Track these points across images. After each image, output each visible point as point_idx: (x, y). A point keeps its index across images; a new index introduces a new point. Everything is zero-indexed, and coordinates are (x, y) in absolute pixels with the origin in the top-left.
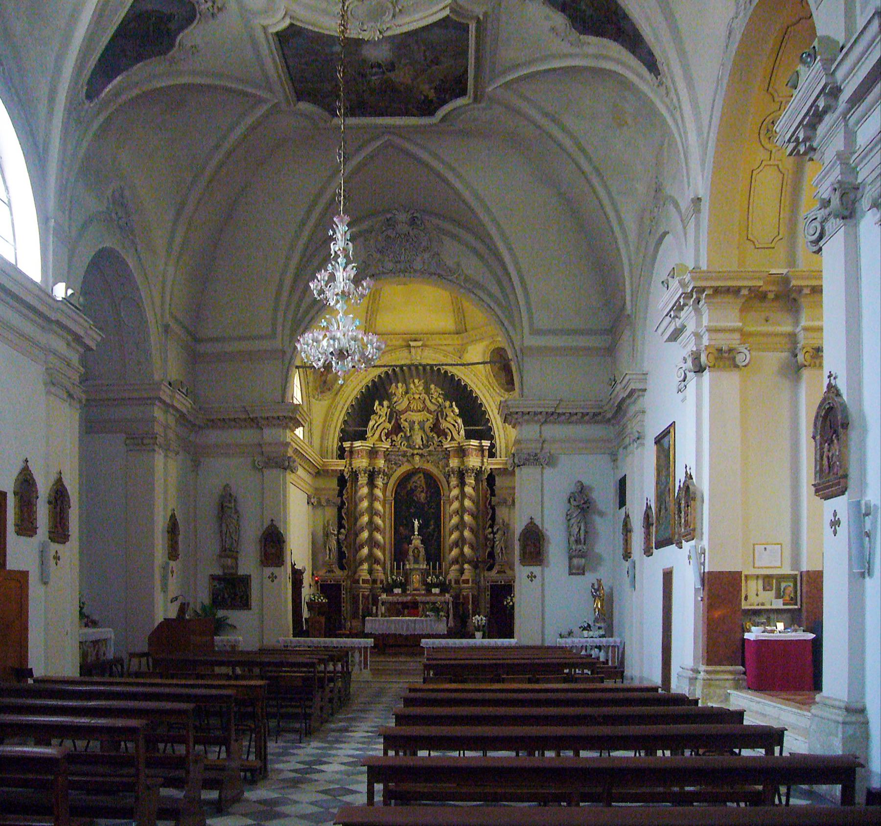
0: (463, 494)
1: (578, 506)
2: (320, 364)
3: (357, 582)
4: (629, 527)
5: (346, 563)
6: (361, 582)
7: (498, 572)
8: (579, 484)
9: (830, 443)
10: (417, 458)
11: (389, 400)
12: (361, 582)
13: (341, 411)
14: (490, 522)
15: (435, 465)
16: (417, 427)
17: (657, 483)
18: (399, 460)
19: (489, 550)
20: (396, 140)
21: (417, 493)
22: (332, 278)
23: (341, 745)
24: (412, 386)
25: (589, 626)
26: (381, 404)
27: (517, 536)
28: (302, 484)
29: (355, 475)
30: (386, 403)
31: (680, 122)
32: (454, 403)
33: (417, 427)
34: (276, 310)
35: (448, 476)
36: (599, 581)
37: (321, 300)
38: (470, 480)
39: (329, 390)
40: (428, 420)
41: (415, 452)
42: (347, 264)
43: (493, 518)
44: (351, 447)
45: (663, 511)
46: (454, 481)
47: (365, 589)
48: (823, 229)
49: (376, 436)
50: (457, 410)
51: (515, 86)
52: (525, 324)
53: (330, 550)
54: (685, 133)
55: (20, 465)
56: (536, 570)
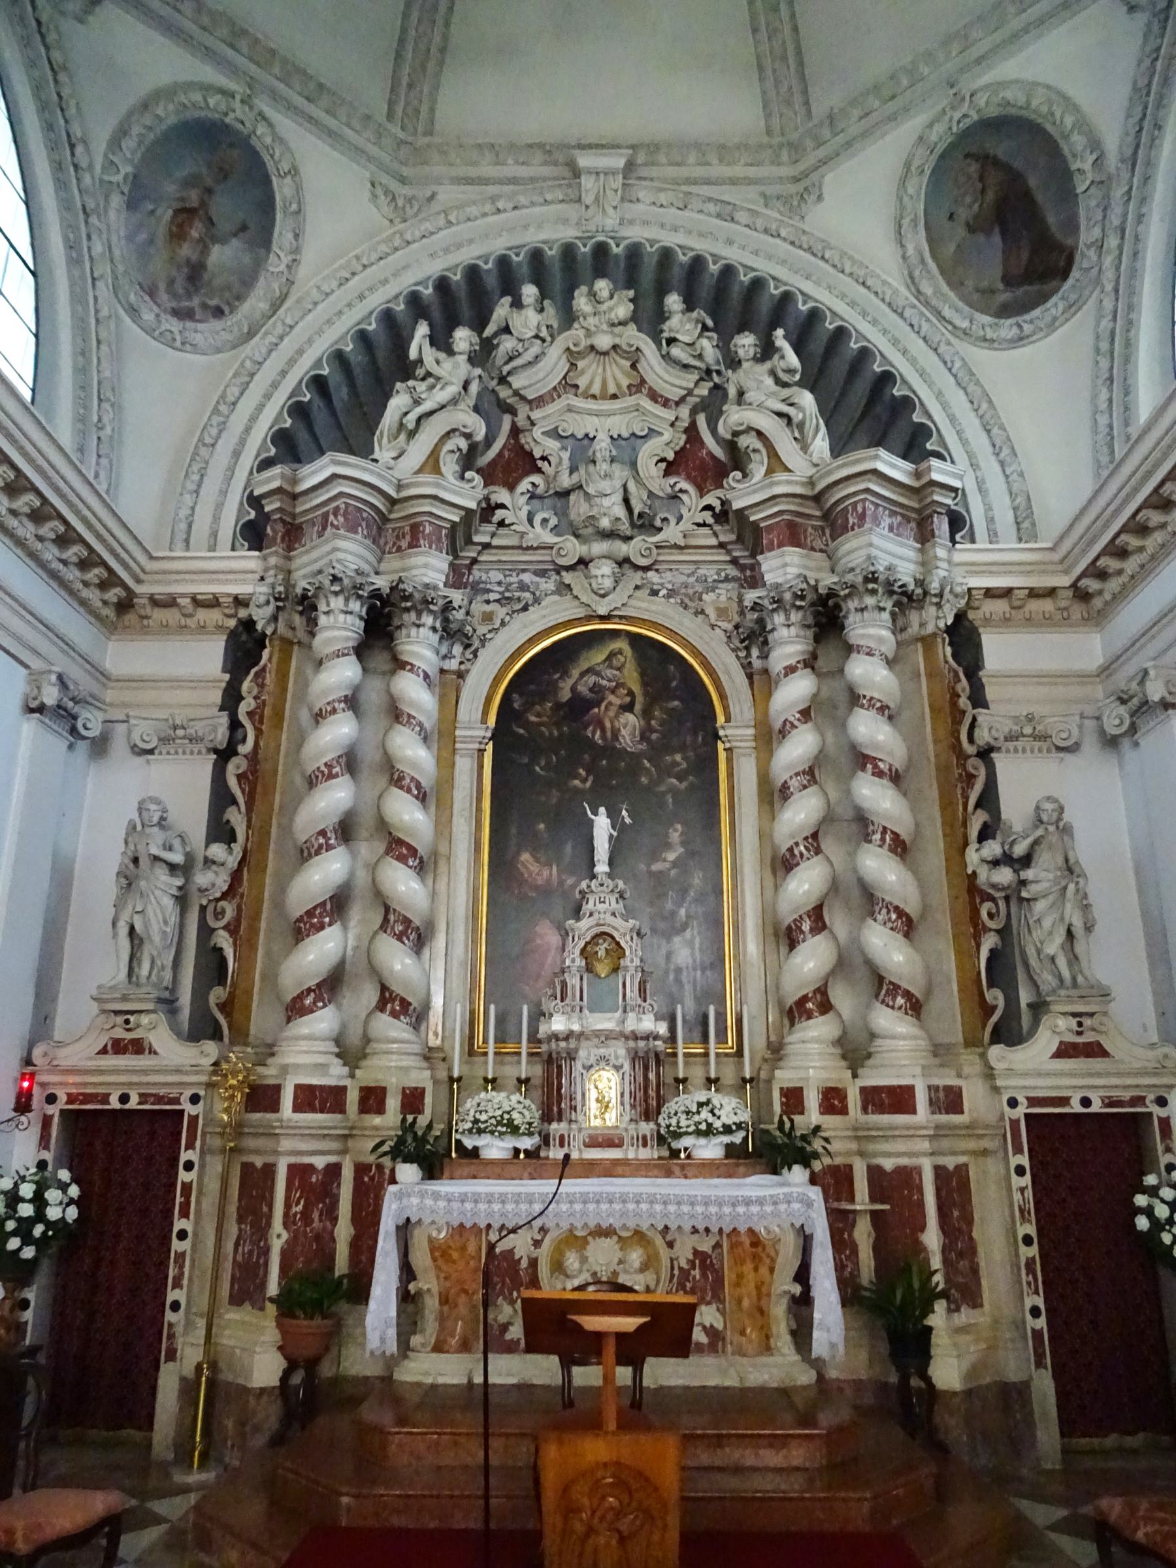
5: (224, 1007)
7: (1065, 1051)
8: (1049, 806)
12: (287, 1099)
13: (268, 396)
18: (523, 587)
19: (989, 942)
24: (581, 302)
30: (463, 338)
39: (219, 313)
40: (652, 433)
43: (989, 799)
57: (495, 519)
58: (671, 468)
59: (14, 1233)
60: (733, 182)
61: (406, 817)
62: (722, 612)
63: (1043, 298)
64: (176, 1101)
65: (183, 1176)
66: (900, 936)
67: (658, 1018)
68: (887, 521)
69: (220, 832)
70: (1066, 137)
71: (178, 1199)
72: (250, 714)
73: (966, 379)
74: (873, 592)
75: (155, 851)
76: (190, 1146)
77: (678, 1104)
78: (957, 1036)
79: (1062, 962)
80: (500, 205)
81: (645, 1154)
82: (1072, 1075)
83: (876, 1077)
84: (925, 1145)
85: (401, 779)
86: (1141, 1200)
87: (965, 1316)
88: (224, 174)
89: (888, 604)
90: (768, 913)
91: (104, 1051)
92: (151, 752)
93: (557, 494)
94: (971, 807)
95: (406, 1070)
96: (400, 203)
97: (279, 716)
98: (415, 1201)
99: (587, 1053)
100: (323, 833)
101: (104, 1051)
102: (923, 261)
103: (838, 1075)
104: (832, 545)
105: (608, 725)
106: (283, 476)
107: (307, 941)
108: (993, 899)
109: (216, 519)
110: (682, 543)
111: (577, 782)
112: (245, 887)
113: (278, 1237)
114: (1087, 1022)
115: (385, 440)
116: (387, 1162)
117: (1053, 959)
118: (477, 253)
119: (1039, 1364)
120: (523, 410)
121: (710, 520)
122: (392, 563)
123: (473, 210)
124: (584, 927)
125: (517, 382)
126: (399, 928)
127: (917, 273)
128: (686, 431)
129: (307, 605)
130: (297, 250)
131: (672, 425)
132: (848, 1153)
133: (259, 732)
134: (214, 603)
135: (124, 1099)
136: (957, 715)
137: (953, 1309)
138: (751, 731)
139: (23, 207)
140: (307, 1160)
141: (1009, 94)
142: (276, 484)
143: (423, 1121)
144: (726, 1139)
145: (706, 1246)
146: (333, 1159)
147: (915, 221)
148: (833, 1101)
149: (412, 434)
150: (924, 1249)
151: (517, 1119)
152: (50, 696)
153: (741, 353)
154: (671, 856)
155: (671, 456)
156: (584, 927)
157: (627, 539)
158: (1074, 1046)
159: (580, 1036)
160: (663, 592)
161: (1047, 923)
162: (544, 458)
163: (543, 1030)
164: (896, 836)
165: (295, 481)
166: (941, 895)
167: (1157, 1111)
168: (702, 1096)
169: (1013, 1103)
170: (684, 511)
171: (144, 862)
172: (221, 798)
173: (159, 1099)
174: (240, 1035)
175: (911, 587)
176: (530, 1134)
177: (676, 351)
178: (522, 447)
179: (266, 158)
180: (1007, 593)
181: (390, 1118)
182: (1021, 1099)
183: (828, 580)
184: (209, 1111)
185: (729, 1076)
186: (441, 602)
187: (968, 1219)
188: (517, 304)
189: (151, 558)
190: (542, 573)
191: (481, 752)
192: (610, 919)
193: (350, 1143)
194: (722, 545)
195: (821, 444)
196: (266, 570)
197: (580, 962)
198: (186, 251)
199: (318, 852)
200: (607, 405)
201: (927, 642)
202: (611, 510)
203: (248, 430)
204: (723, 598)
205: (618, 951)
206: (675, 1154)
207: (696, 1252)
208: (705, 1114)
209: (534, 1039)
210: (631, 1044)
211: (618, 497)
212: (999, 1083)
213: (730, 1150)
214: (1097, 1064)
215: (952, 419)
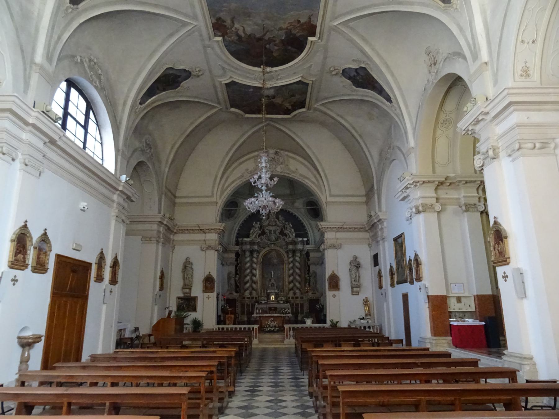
0: (294, 260)
1: (355, 266)
2: (255, 210)
4: (381, 275)
5: (239, 290)
9: (499, 244)
10: (273, 245)
14: (307, 272)
16: (272, 232)
17: (396, 257)
20: (272, 123)
22: (260, 177)
23: (262, 377)
25: (363, 317)
27: (327, 279)
29: (244, 252)
30: (258, 223)
31: (402, 119)
33: (272, 232)
34: (213, 187)
36: (366, 298)
37: (255, 186)
40: (278, 230)
41: (272, 242)
42: (266, 172)
43: (309, 270)
45: (400, 269)
47: (247, 302)
48: (483, 162)
49: (254, 236)
50: (291, 226)
51: (325, 105)
52: (328, 193)
53: (231, 284)
54: (405, 124)
55: (99, 251)
56: (336, 293)
73: (310, 224)
77: (280, 298)
103: (293, 296)
148: (292, 298)
156: (271, 283)
172: (236, 270)
174: (240, 293)
183: (294, 249)
205: (274, 285)
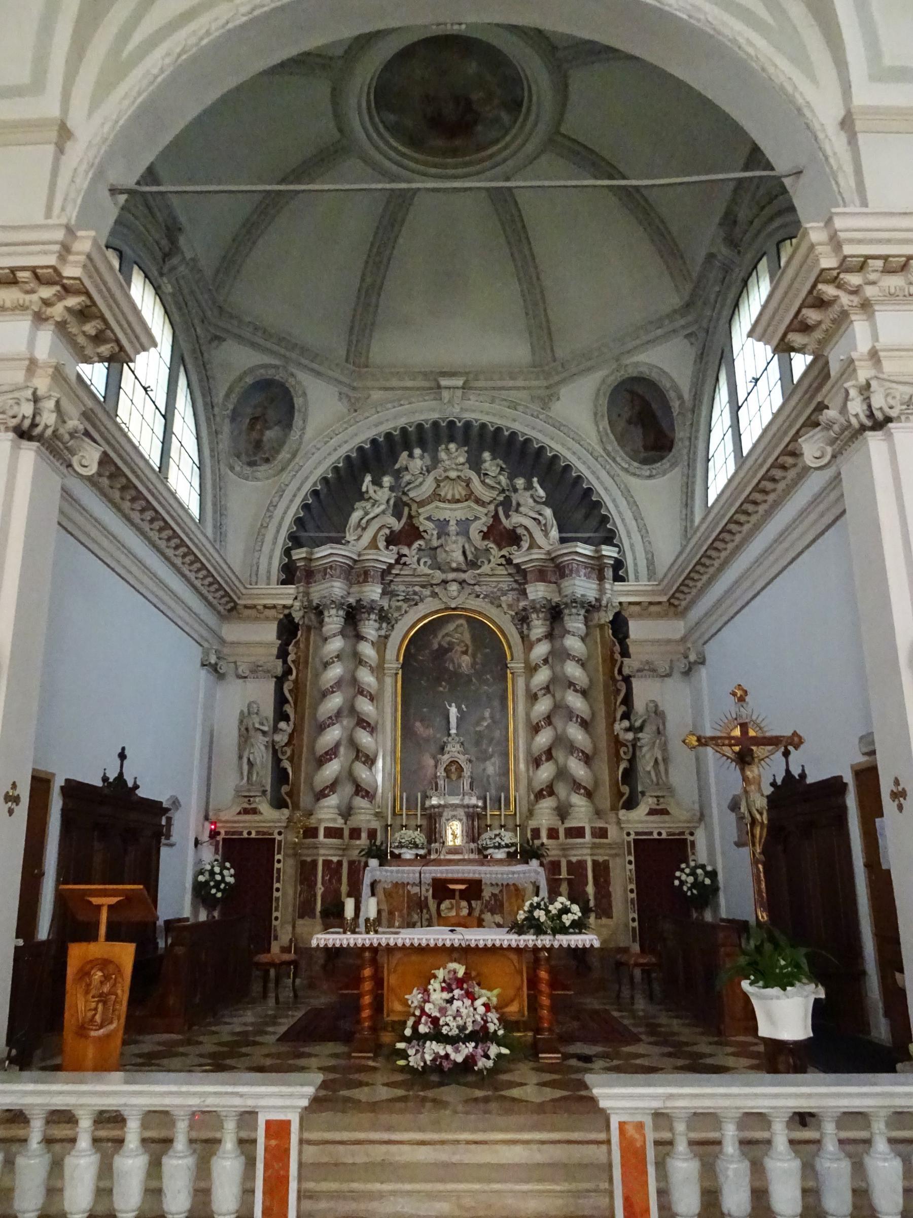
3: (312, 832)
6: (321, 832)
7: (652, 812)
8: (652, 705)
10: (454, 588)
11: (397, 475)
12: (321, 832)
13: (292, 501)
15: (492, 603)
18: (415, 593)
19: (623, 765)
21: (455, 655)
24: (443, 455)
26: (377, 482)
28: (180, 611)
30: (387, 480)
32: (535, 479)
35: (522, 619)
38: (575, 623)
39: (267, 460)
43: (628, 700)
44: (309, 560)
46: (538, 628)
57: (402, 562)
58: (485, 536)
59: (214, 887)
60: (517, 388)
61: (365, 708)
62: (510, 606)
63: (662, 458)
64: (272, 834)
65: (277, 865)
66: (582, 763)
67: (478, 798)
68: (582, 572)
69: (281, 715)
70: (668, 391)
71: (275, 875)
72: (293, 662)
73: (627, 493)
74: (575, 607)
75: (257, 726)
76: (279, 853)
78: (608, 804)
79: (653, 774)
80: (402, 402)
81: (472, 856)
82: (652, 822)
83: (572, 823)
84: (588, 851)
85: (363, 691)
86: (678, 874)
87: (604, 920)
88: (272, 400)
89: (582, 612)
90: (529, 751)
91: (239, 813)
92: (246, 677)
93: (430, 548)
94: (618, 703)
95: (369, 821)
96: (353, 400)
97: (306, 662)
98: (378, 873)
99: (447, 814)
100: (330, 718)
101: (239, 813)
102: (607, 434)
103: (555, 822)
104: (559, 581)
105: (456, 661)
106: (307, 552)
107: (324, 767)
108: (626, 746)
109: (270, 564)
110: (490, 573)
111: (441, 689)
112: (294, 742)
113: (320, 889)
114: (662, 800)
115: (351, 530)
116: (363, 859)
117: (649, 772)
118: (392, 426)
119: (634, 941)
120: (414, 507)
121: (504, 563)
122: (355, 589)
123: (389, 406)
124: (446, 758)
125: (412, 494)
126: (363, 759)
127: (604, 440)
128: (493, 517)
129: (319, 611)
130: (304, 428)
131: (486, 515)
132: (558, 855)
133: (297, 669)
134: (274, 607)
135: (249, 833)
136: (613, 661)
137: (598, 917)
138: (523, 665)
139: (196, 441)
140: (330, 858)
141: (641, 369)
142: (304, 555)
143: (378, 843)
144: (507, 850)
145: (496, 891)
146: (340, 858)
147: (603, 416)
148: (553, 833)
149: (364, 529)
150: (587, 894)
151: (418, 841)
152: (213, 660)
153: (518, 487)
154: (485, 724)
155: (485, 529)
156: (446, 758)
157: (465, 572)
158: (655, 810)
159: (444, 806)
160: (482, 596)
161: (648, 756)
162: (425, 531)
163: (427, 804)
164: (582, 718)
165: (312, 553)
166: (603, 744)
167: (690, 838)
168: (497, 832)
169: (628, 834)
170: (492, 558)
171: (252, 732)
172: (280, 700)
173: (264, 833)
174: (296, 806)
175: (593, 603)
176: (423, 848)
177: (487, 481)
178: (414, 525)
179: (291, 389)
180: (638, 603)
181: (364, 841)
182: (632, 832)
183: (556, 599)
184: (285, 838)
185: (511, 825)
186: (378, 608)
187: (607, 882)
188: (411, 456)
189: (246, 588)
190: (423, 586)
191: (397, 674)
192: (456, 754)
193: (346, 852)
194: (510, 574)
195: (554, 533)
196: (298, 593)
197: (444, 774)
198: (255, 435)
199: (329, 726)
200: (454, 506)
201: (601, 627)
202: (457, 557)
203: (283, 518)
204: (510, 599)
206: (486, 857)
207: (492, 894)
208: (498, 839)
209: (423, 808)
210: (466, 810)
211: (460, 552)
212: (623, 826)
213: (509, 853)
214: (666, 818)
215: (620, 513)
